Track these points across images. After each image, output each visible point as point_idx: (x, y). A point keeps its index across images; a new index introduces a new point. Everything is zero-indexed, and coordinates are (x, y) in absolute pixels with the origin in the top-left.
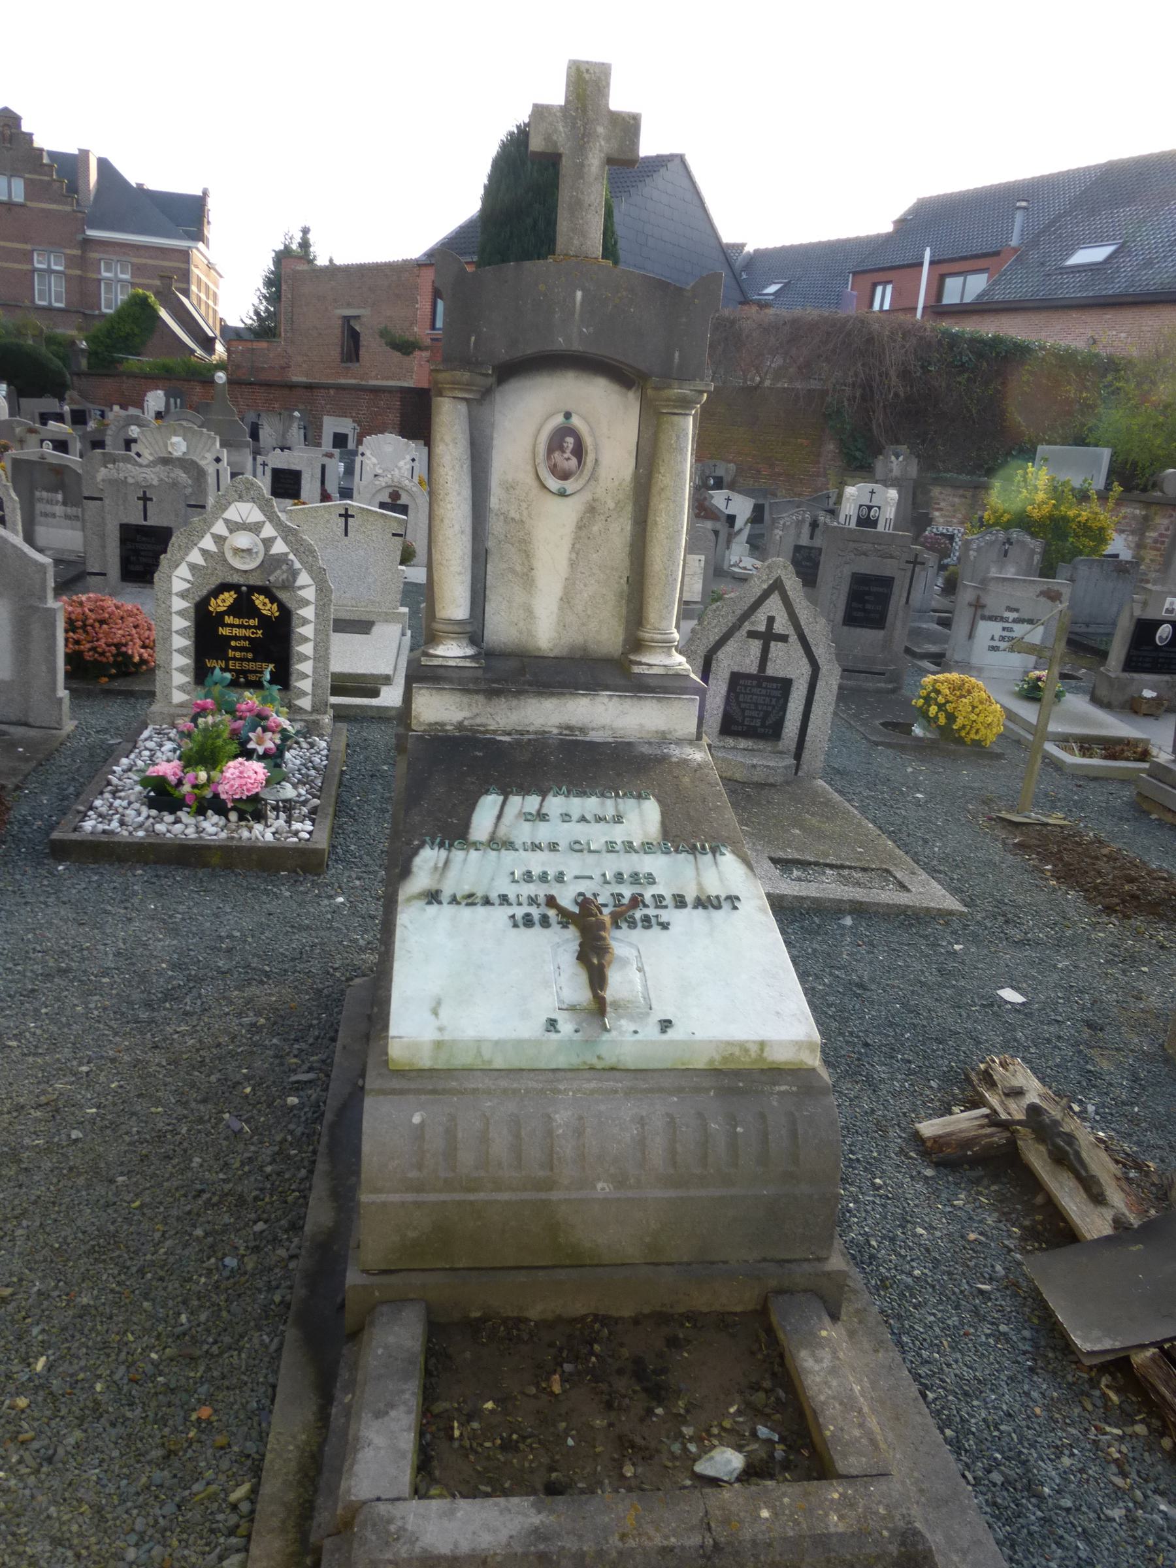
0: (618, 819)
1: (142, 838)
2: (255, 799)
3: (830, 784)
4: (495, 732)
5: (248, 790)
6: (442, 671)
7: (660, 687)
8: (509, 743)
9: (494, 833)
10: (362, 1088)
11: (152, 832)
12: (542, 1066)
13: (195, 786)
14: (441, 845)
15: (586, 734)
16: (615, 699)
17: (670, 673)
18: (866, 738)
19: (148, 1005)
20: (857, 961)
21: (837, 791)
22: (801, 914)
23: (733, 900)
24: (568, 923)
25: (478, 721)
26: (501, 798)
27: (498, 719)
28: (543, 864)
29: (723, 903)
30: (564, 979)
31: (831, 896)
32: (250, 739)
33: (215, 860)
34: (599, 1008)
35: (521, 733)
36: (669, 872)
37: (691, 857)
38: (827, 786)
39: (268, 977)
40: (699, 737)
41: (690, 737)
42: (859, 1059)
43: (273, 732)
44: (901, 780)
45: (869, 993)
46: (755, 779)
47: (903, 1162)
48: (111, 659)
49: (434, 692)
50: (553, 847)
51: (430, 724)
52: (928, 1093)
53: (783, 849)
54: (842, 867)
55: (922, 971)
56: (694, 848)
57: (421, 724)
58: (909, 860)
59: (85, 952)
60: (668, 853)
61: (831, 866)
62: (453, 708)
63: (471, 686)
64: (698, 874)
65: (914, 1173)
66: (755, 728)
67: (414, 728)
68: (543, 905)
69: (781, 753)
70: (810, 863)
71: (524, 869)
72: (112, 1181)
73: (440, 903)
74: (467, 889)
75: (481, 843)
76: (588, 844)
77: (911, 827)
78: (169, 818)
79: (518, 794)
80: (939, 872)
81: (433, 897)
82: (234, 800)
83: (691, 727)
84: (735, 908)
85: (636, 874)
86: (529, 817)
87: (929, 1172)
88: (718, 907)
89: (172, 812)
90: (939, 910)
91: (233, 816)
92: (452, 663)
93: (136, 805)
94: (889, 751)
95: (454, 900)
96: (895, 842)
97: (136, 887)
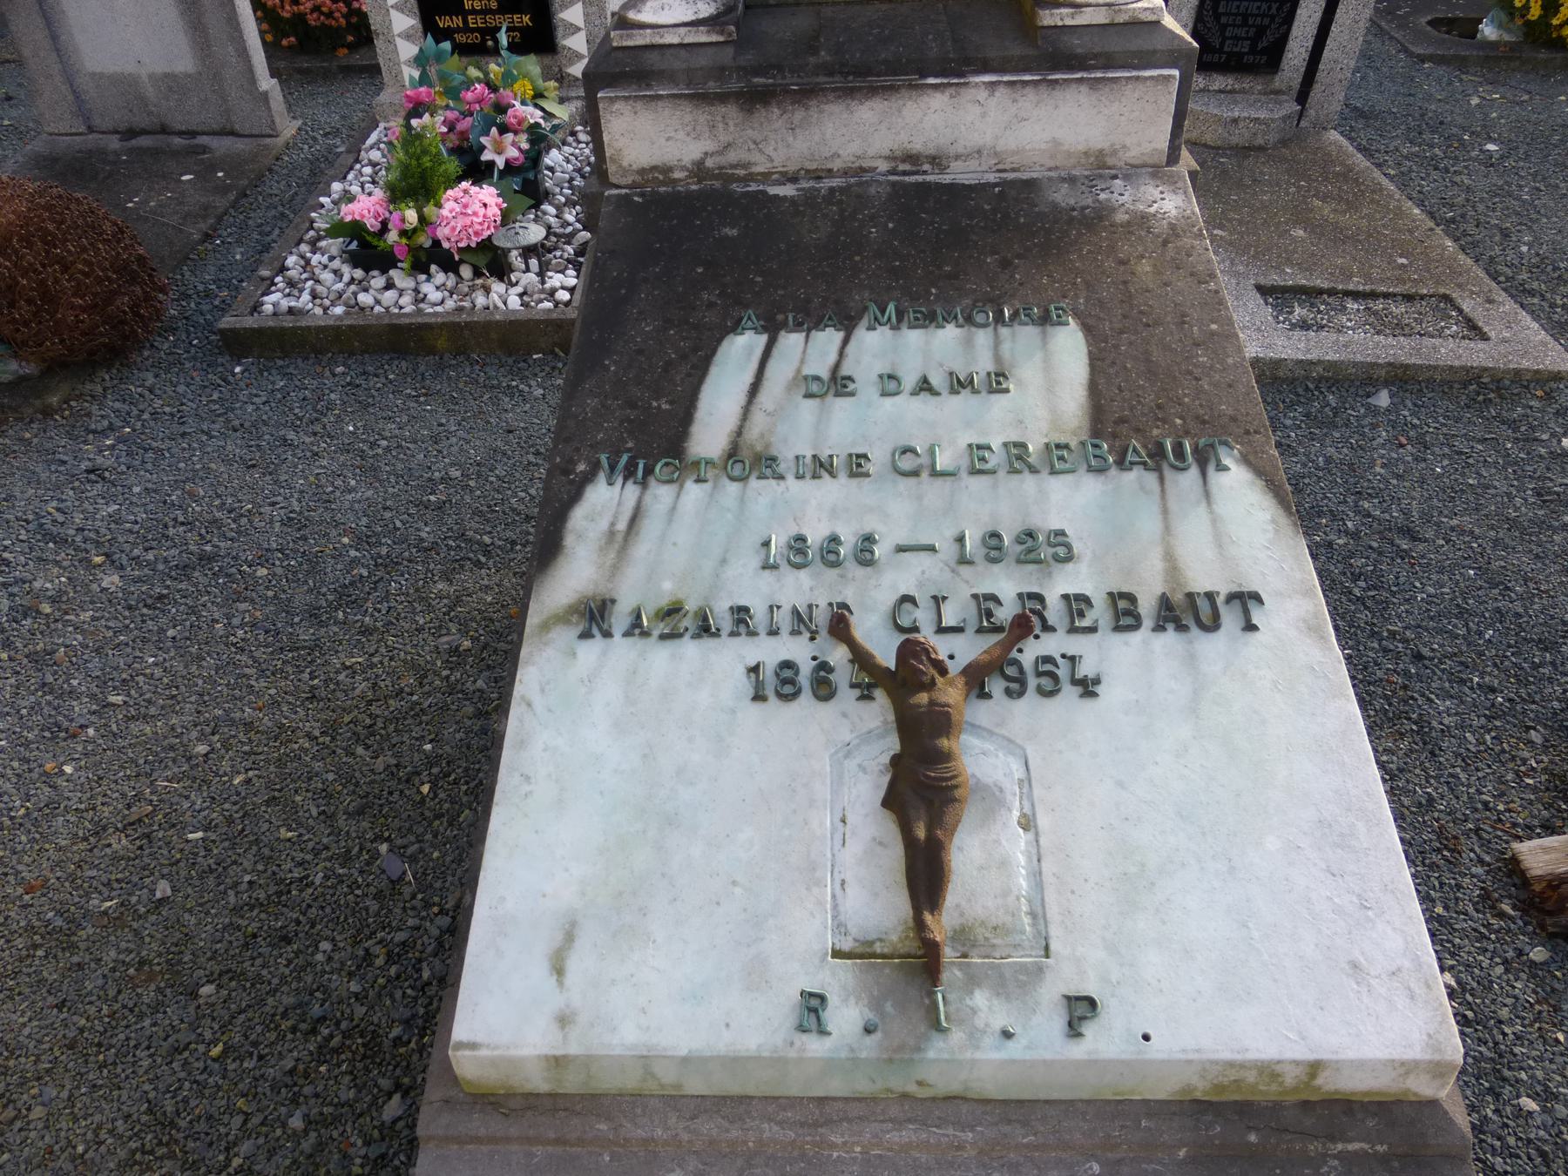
0: (997, 382)
1: (339, 318)
2: (486, 245)
3: (1350, 139)
4: (766, 177)
5: (477, 234)
6: (653, 57)
7: (1096, 56)
8: (792, 201)
9: (739, 432)
10: (416, 1139)
11: (355, 307)
12: (795, 1091)
13: (403, 233)
14: (629, 473)
15: (943, 169)
16: (1001, 92)
17: (1121, 19)
18: (1406, 51)
19: (313, 614)
20: (1398, 477)
21: (1361, 149)
22: (1307, 389)
23: (1246, 600)
24: (870, 686)
25: (733, 156)
26: (764, 338)
27: (769, 150)
28: (834, 513)
29: (1223, 609)
30: (851, 854)
31: (1359, 358)
32: (483, 148)
33: (441, 343)
34: (916, 965)
35: (817, 175)
36: (1106, 524)
37: (1151, 479)
38: (1345, 142)
39: (487, 553)
40: (1173, 158)
41: (1155, 160)
42: (1405, 687)
43: (516, 133)
44: (1460, 120)
45: (1421, 546)
46: (1235, 140)
47: (1488, 926)
48: (343, 21)
49: (639, 105)
50: (857, 465)
51: (642, 172)
52: (1526, 754)
53: (1279, 268)
54: (1373, 295)
55: (1508, 495)
56: (1158, 453)
57: (625, 171)
58: (1482, 274)
59: (244, 521)
60: (1100, 471)
61: (1356, 295)
62: (681, 135)
63: (712, 87)
64: (1167, 529)
65: (1511, 954)
66: (1241, 55)
67: (613, 180)
68: (824, 633)
69: (1278, 92)
70: (1321, 292)
71: (794, 530)
72: (194, 995)
73: (607, 634)
74: (667, 589)
75: (709, 462)
76: (932, 452)
77: (1481, 208)
78: (378, 281)
79: (798, 327)
80: (1532, 293)
81: (593, 616)
82: (460, 250)
83: (1160, 137)
84: (1250, 627)
85: (1030, 534)
86: (815, 388)
87: (1538, 954)
88: (1212, 625)
89: (384, 271)
90: (1537, 372)
91: (466, 271)
92: (671, 38)
93: (336, 264)
94: (1441, 71)
95: (636, 628)
96: (1456, 240)
97: (333, 396)
